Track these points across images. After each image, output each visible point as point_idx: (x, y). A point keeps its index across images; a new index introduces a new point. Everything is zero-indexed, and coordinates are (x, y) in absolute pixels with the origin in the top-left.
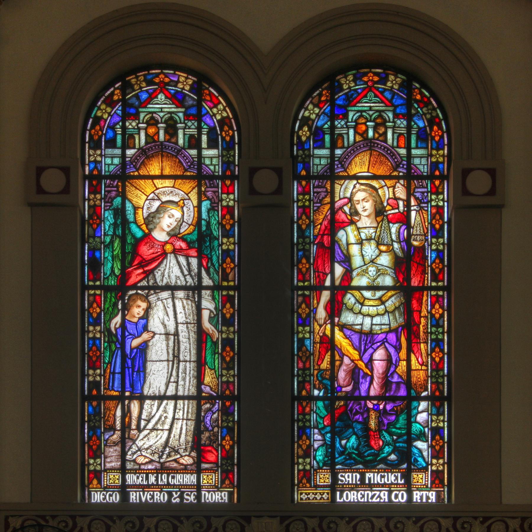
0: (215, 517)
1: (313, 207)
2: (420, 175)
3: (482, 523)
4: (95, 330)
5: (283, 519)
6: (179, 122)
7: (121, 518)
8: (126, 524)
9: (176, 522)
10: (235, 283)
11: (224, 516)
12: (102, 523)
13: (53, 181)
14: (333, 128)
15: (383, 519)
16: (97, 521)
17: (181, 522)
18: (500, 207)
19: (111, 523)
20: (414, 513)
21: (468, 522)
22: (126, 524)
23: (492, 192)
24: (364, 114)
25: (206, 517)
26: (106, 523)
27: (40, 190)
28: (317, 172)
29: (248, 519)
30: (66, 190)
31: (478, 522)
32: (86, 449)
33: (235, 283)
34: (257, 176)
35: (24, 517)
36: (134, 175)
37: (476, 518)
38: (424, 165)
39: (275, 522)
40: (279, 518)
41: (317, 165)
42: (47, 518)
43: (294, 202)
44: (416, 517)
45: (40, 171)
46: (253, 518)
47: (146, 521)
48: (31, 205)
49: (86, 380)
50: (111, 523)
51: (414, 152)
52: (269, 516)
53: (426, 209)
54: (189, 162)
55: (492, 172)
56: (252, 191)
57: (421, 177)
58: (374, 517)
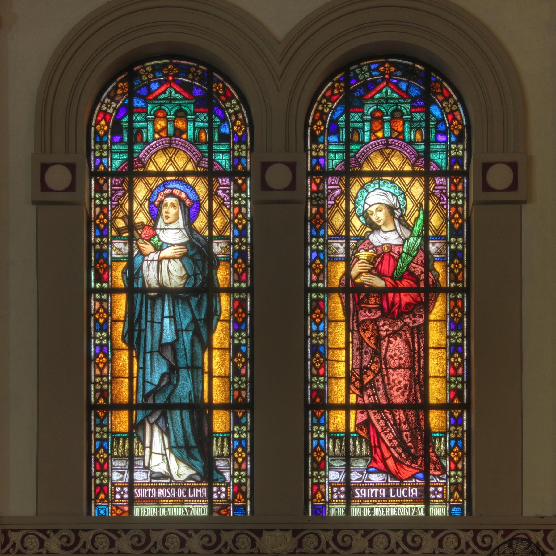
0: (153, 530)
1: (328, 204)
2: (222, 171)
3: (434, 536)
4: (456, 335)
5: (295, 533)
6: (189, 112)
7: (126, 531)
8: (61, 538)
9: (41, 535)
10: (463, 285)
11: (93, 530)
12: (176, 536)
13: (58, 177)
14: (347, 121)
15: (330, 532)
16: (243, 536)
17: (119, 536)
18: (521, 202)
19: (44, 537)
20: (429, 525)
21: (489, 536)
22: (61, 538)
23: (514, 187)
24: (163, 107)
25: (73, 530)
26: (181, 538)
27: (45, 188)
28: (332, 168)
29: (259, 533)
30: (72, 188)
31: (359, 536)
32: (310, 461)
33: (463, 285)
34: (492, 171)
35: (95, 531)
36: (138, 172)
37: (427, 531)
38: (442, 159)
39: (289, 534)
40: (291, 531)
41: (333, 160)
42: (48, 532)
43: (250, 198)
44: (434, 530)
45: (45, 167)
46: (264, 532)
47: (82, 535)
48: (34, 203)
49: (309, 387)
50: (44, 537)
51: (216, 147)
52: (281, 530)
53: (445, 206)
54: (198, 157)
55: (514, 166)
56: (265, 187)
57: (223, 174)
58: (392, 530)
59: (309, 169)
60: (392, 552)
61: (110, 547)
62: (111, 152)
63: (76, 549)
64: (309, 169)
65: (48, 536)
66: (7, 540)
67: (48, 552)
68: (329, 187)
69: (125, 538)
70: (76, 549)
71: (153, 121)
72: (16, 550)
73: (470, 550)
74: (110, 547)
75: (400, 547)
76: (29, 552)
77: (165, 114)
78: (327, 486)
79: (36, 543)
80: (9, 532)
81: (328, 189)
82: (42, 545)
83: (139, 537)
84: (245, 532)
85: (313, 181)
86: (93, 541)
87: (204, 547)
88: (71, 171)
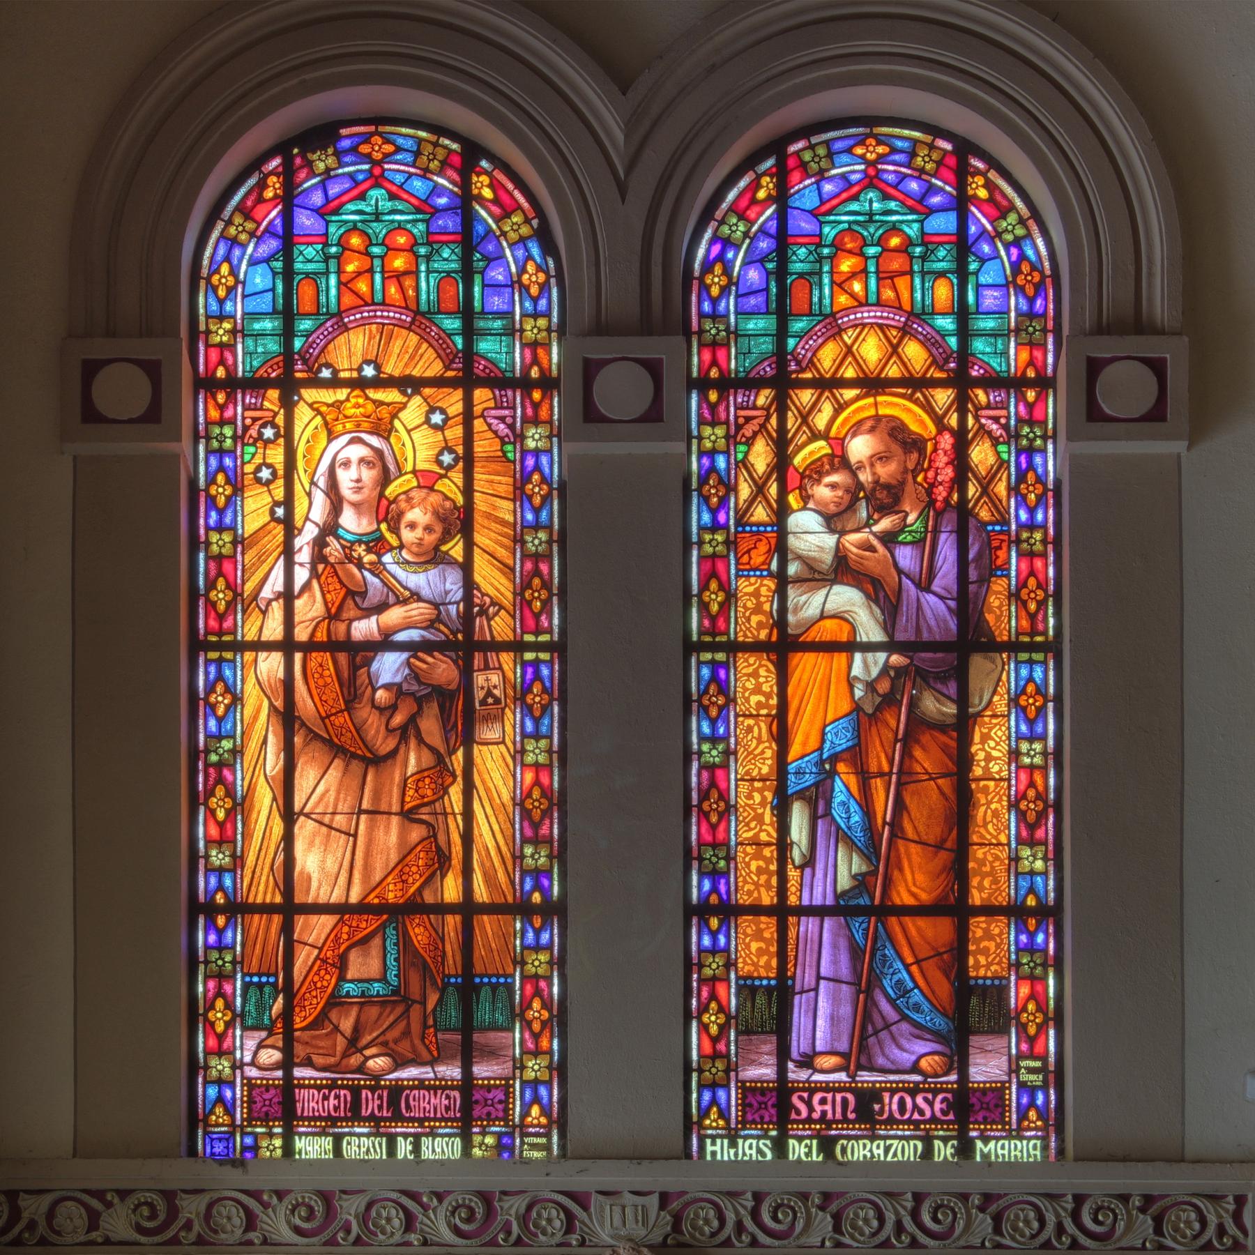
22: (137, 1207)
59: (695, 374)
60: (1047, 1245)
61: (246, 1231)
62: (244, 336)
63: (170, 1233)
64: (695, 374)
65: (266, 1206)
66: (15, 1214)
67: (265, 1242)
68: (248, 414)
69: (283, 1209)
70: (170, 1233)
71: (832, 258)
72: (352, 1237)
73: (745, 1238)
74: (246, 1231)
75: (746, 1230)
76: (68, 1239)
77: (412, 241)
78: (1014, 1105)
79: (238, 1219)
80: (594, 1197)
81: (736, 417)
82: (93, 1225)
83: (151, 1206)
84: (70, 1194)
85: (703, 397)
86: (51, 1215)
87: (298, 1231)
88: (152, 384)
